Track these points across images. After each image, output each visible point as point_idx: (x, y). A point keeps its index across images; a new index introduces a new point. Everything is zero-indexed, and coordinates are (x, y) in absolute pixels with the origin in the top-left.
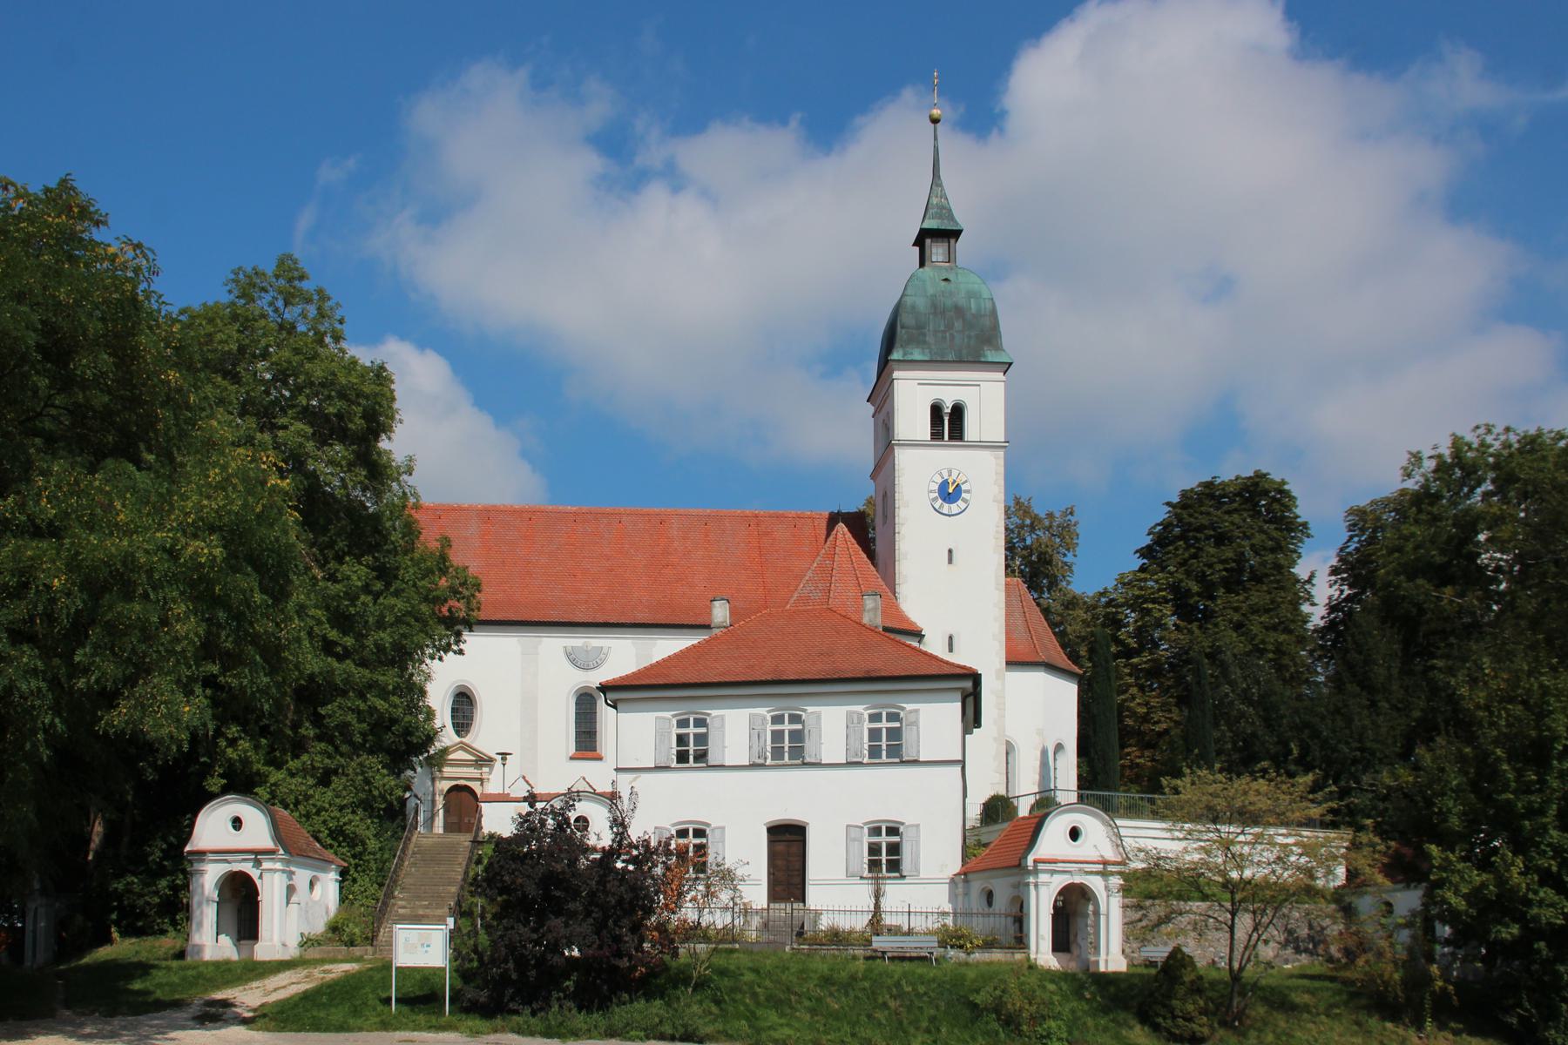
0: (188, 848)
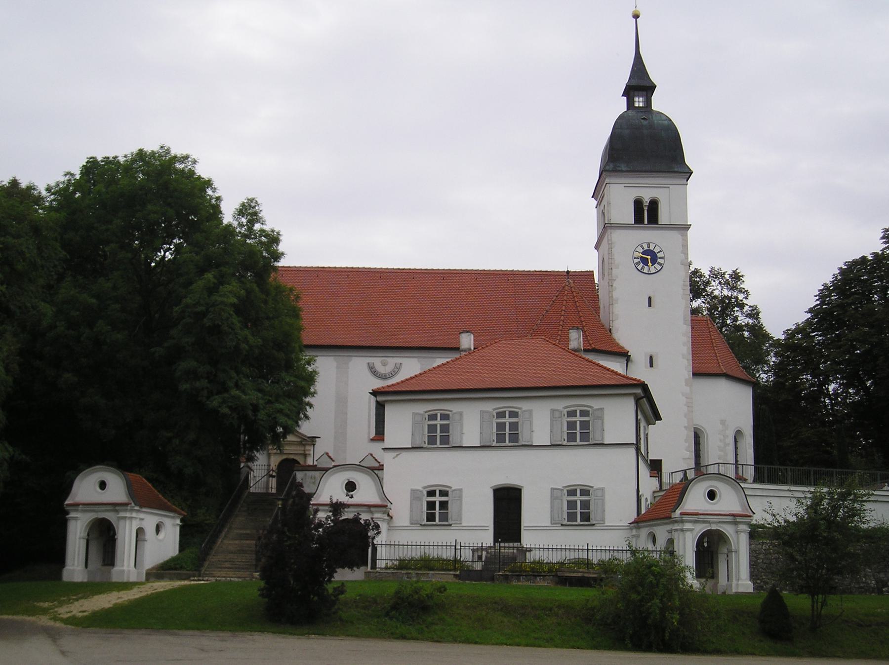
0: (67, 502)
